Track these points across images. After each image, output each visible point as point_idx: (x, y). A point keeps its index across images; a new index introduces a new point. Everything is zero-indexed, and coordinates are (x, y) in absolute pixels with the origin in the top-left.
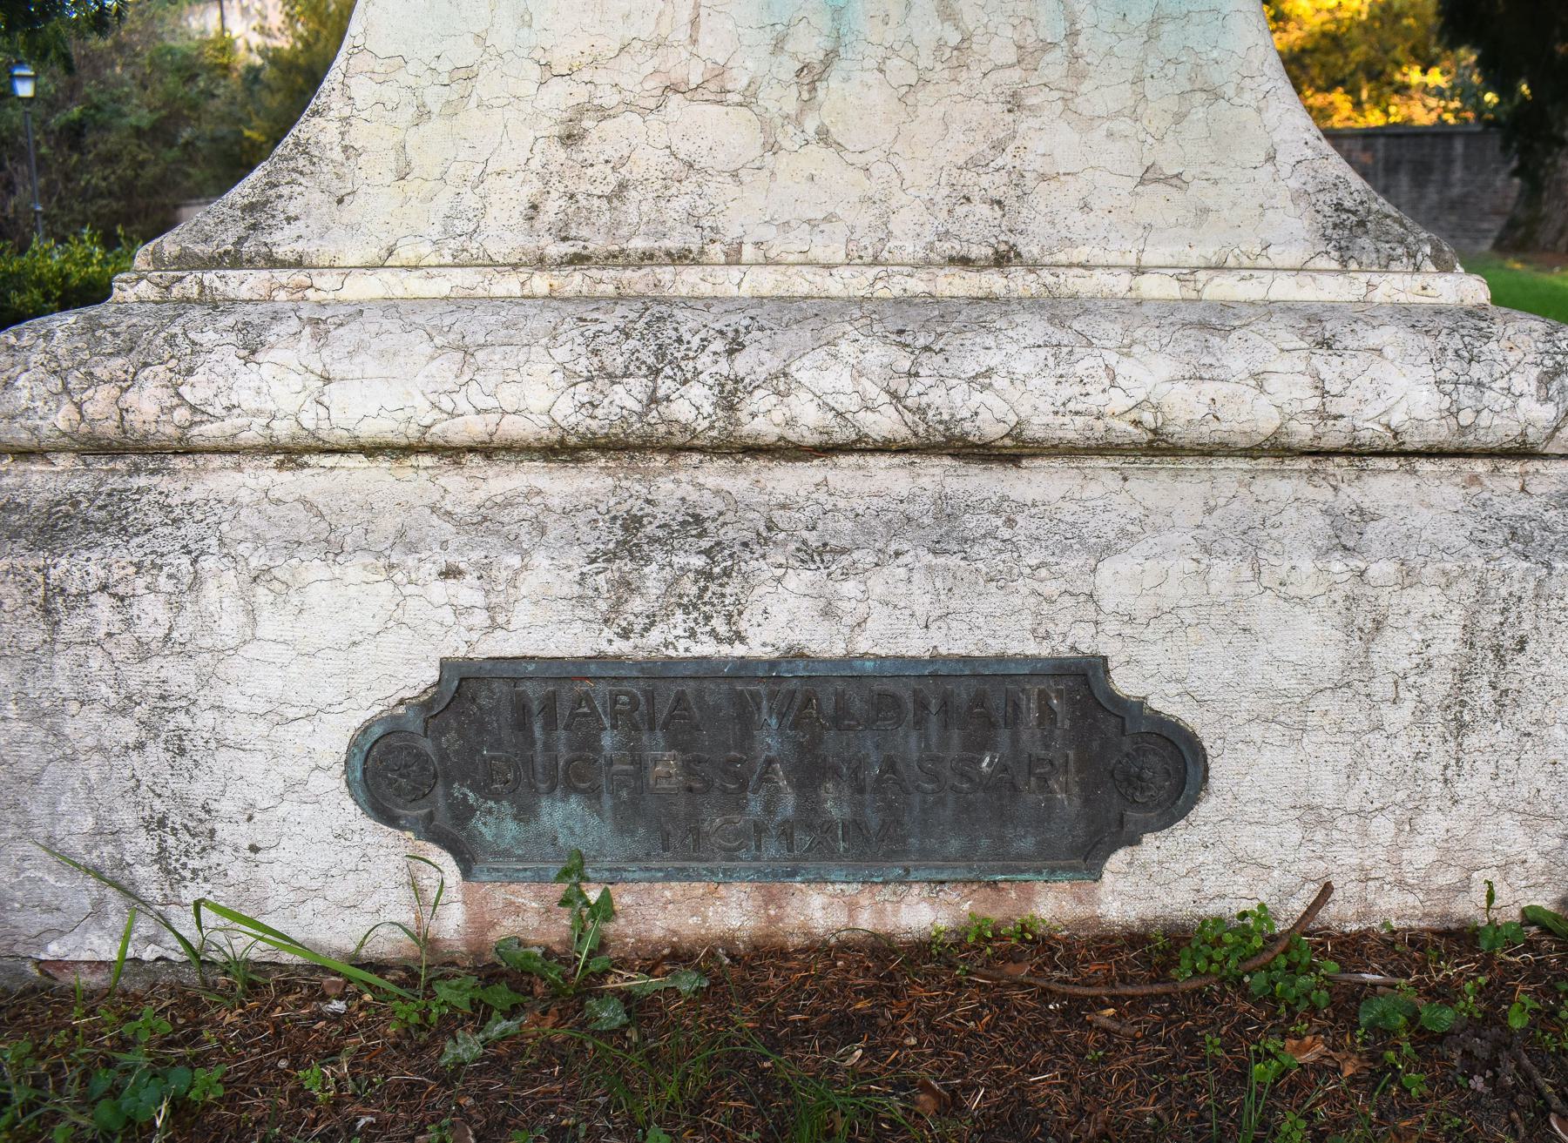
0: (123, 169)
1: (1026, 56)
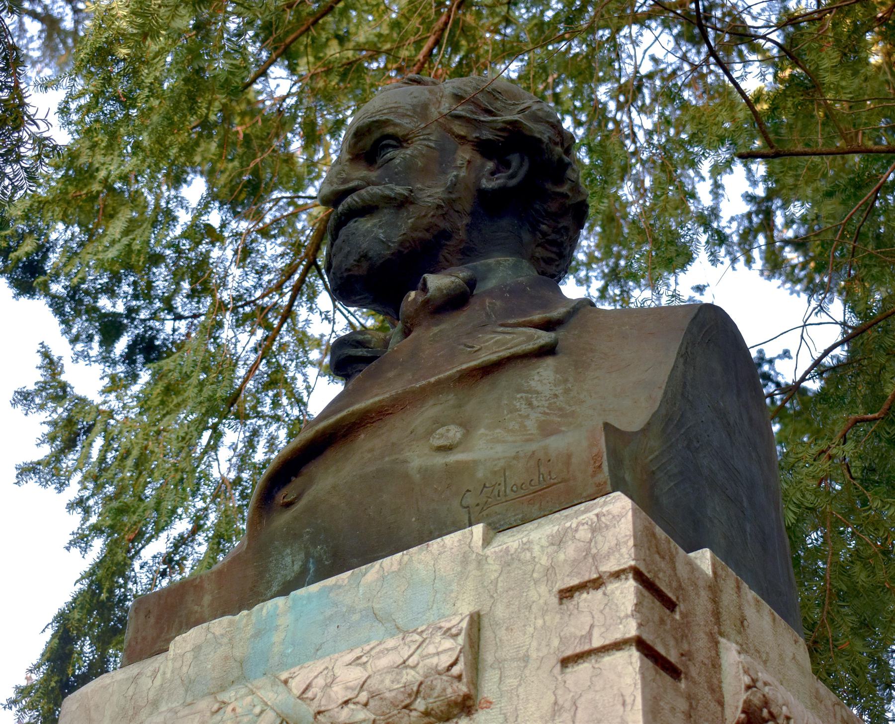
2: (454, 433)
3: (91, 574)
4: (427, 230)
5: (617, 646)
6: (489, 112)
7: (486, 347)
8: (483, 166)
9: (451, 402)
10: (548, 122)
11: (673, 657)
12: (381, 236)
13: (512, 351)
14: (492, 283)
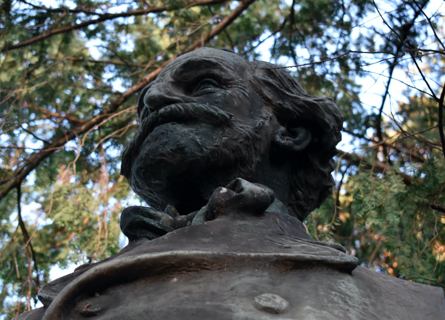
4: (233, 151)
7: (294, 247)
8: (278, 127)
9: (266, 279)
10: (334, 116)
12: (198, 140)
13: (324, 257)
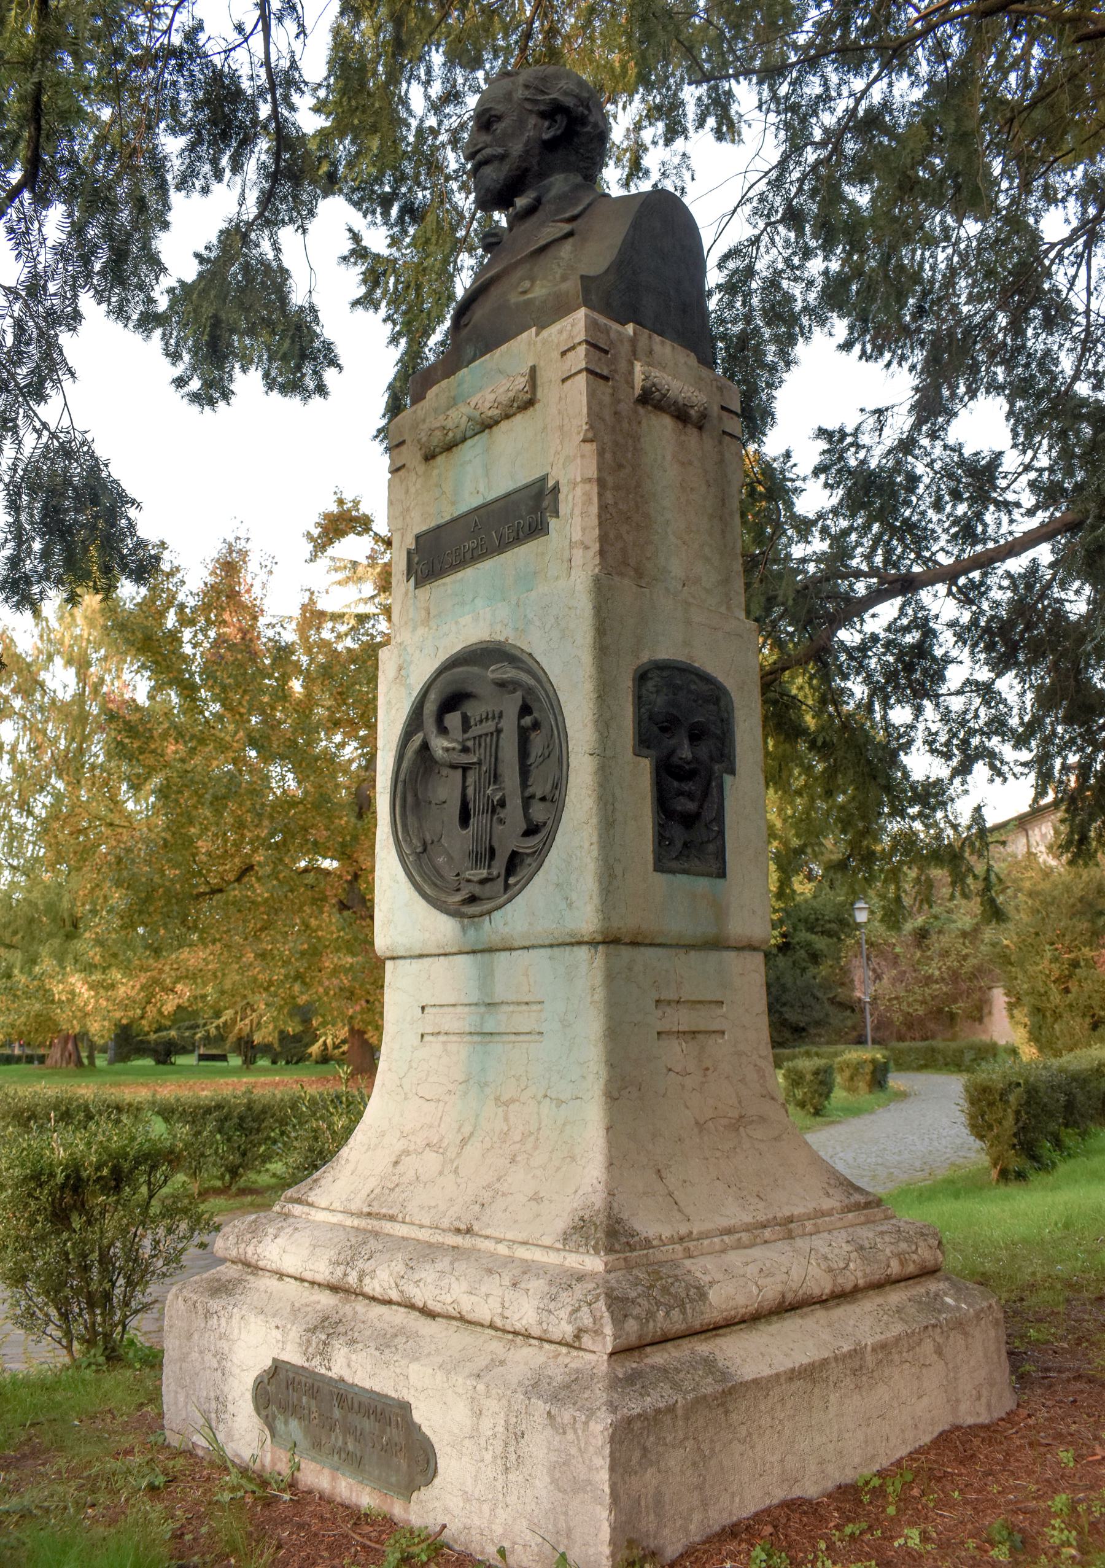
0: (952, 962)
1: (525, 1136)
2: (527, 284)
3: (400, 361)
5: (579, 372)
6: (543, 92)
11: (605, 373)
14: (553, 193)
